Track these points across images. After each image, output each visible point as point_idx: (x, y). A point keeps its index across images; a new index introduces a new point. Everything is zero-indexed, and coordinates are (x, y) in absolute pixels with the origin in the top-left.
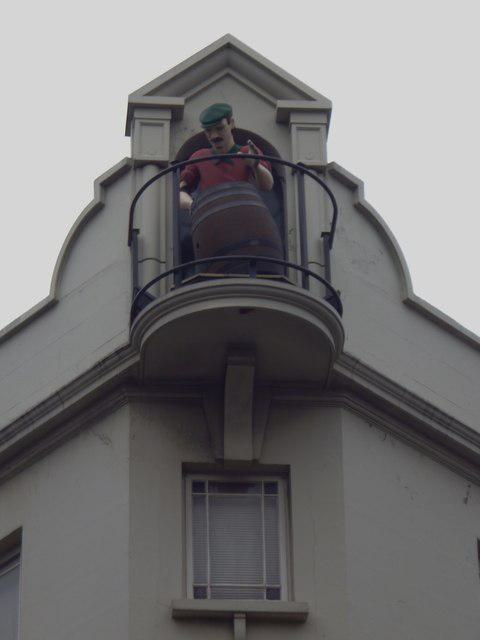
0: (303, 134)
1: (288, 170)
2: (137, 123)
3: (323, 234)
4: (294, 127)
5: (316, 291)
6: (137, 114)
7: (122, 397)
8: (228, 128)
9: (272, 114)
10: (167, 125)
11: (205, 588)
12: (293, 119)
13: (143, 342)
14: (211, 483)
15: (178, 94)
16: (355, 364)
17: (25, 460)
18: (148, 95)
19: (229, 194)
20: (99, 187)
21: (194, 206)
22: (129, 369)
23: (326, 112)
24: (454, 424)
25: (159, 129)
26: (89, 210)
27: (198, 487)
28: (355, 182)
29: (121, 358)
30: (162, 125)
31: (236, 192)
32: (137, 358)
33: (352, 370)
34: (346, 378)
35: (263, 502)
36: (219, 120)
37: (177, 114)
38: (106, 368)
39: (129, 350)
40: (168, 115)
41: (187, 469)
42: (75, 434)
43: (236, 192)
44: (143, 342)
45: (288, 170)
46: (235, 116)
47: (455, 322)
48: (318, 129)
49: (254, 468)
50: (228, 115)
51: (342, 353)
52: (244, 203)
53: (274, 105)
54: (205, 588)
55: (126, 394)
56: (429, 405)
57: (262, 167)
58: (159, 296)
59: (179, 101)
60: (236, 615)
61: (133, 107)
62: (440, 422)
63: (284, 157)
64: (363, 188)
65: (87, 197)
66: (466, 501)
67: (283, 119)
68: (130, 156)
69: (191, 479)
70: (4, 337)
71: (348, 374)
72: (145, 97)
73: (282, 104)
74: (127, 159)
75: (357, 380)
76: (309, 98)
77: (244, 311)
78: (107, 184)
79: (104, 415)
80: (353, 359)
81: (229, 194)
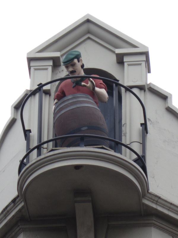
0: (131, 68)
1: (123, 90)
2: (32, 69)
3: (142, 124)
4: (126, 64)
5: (128, 157)
6: (32, 64)
7: (18, 228)
8: (79, 65)
9: (114, 58)
10: (50, 69)
12: (126, 59)
13: (23, 190)
16: (157, 199)
19: (70, 101)
20: (13, 109)
22: (20, 210)
23: (146, 54)
25: (45, 71)
28: (165, 94)
30: (47, 69)
31: (75, 100)
32: (23, 204)
33: (157, 203)
34: (153, 208)
36: (73, 59)
37: (56, 63)
38: (8, 212)
40: (51, 63)
43: (75, 100)
44: (23, 190)
45: (123, 90)
46: (83, 58)
47: (20, 97)
50: (78, 57)
51: (150, 194)
52: (78, 106)
53: (114, 52)
55: (20, 227)
57: (97, 89)
58: (29, 162)
59: (57, 54)
61: (30, 60)
63: (120, 82)
64: (171, 98)
65: (7, 115)
67: (120, 60)
68: (29, 89)
71: (154, 206)
72: (38, 53)
73: (118, 51)
74: (27, 90)
75: (160, 209)
76: (135, 47)
77: (77, 167)
78: (19, 106)
80: (156, 196)
81: (70, 101)
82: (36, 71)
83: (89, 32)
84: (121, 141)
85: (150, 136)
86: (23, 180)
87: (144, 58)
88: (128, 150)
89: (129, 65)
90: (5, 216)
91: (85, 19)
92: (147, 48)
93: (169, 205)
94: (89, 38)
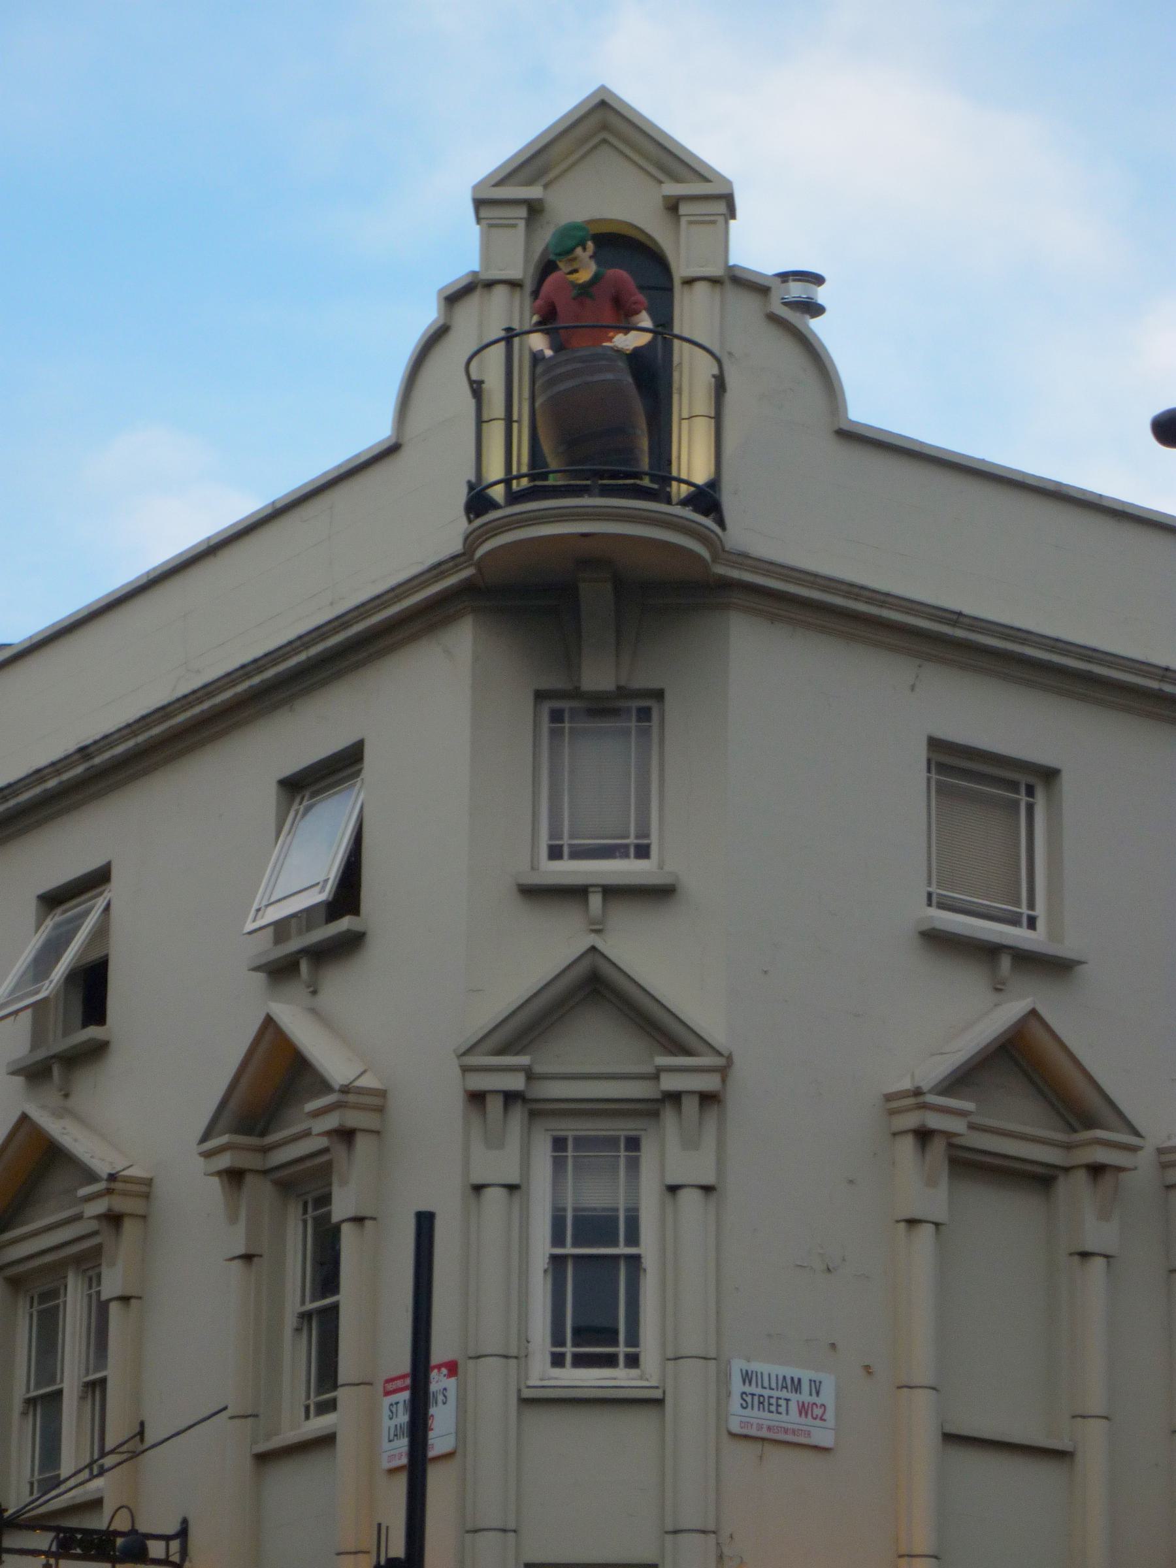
4: (683, 220)
10: (522, 224)
11: (561, 846)
12: (684, 209)
14: (571, 709)
15: (530, 182)
16: (743, 559)
17: (365, 654)
18: (497, 185)
20: (443, 302)
21: (551, 358)
23: (728, 200)
24: (890, 600)
26: (418, 351)
27: (556, 716)
29: (456, 566)
30: (514, 226)
35: (633, 732)
37: (534, 209)
38: (442, 573)
39: (462, 559)
40: (523, 212)
41: (540, 696)
42: (414, 638)
48: (713, 222)
49: (623, 692)
51: (729, 552)
54: (561, 846)
56: (852, 585)
59: (534, 192)
60: (591, 889)
61: (480, 204)
62: (870, 601)
65: (428, 315)
66: (913, 688)
67: (673, 206)
69: (546, 707)
70: (3, 1144)
74: (474, 273)
78: (453, 299)
79: (448, 620)
82: (494, 230)
83: (605, 127)
84: (671, 474)
85: (730, 397)
86: (480, 536)
87: (721, 207)
88: (686, 345)
89: (691, 223)
90: (436, 576)
91: (596, 101)
92: (729, 183)
93: (766, 566)
94: (605, 141)
